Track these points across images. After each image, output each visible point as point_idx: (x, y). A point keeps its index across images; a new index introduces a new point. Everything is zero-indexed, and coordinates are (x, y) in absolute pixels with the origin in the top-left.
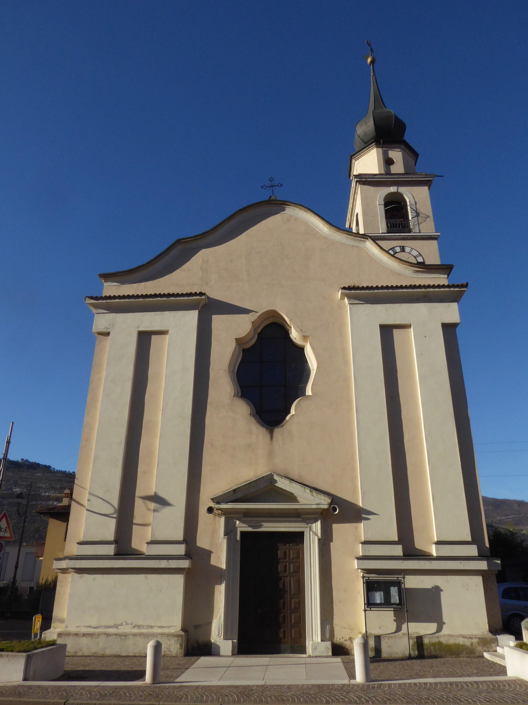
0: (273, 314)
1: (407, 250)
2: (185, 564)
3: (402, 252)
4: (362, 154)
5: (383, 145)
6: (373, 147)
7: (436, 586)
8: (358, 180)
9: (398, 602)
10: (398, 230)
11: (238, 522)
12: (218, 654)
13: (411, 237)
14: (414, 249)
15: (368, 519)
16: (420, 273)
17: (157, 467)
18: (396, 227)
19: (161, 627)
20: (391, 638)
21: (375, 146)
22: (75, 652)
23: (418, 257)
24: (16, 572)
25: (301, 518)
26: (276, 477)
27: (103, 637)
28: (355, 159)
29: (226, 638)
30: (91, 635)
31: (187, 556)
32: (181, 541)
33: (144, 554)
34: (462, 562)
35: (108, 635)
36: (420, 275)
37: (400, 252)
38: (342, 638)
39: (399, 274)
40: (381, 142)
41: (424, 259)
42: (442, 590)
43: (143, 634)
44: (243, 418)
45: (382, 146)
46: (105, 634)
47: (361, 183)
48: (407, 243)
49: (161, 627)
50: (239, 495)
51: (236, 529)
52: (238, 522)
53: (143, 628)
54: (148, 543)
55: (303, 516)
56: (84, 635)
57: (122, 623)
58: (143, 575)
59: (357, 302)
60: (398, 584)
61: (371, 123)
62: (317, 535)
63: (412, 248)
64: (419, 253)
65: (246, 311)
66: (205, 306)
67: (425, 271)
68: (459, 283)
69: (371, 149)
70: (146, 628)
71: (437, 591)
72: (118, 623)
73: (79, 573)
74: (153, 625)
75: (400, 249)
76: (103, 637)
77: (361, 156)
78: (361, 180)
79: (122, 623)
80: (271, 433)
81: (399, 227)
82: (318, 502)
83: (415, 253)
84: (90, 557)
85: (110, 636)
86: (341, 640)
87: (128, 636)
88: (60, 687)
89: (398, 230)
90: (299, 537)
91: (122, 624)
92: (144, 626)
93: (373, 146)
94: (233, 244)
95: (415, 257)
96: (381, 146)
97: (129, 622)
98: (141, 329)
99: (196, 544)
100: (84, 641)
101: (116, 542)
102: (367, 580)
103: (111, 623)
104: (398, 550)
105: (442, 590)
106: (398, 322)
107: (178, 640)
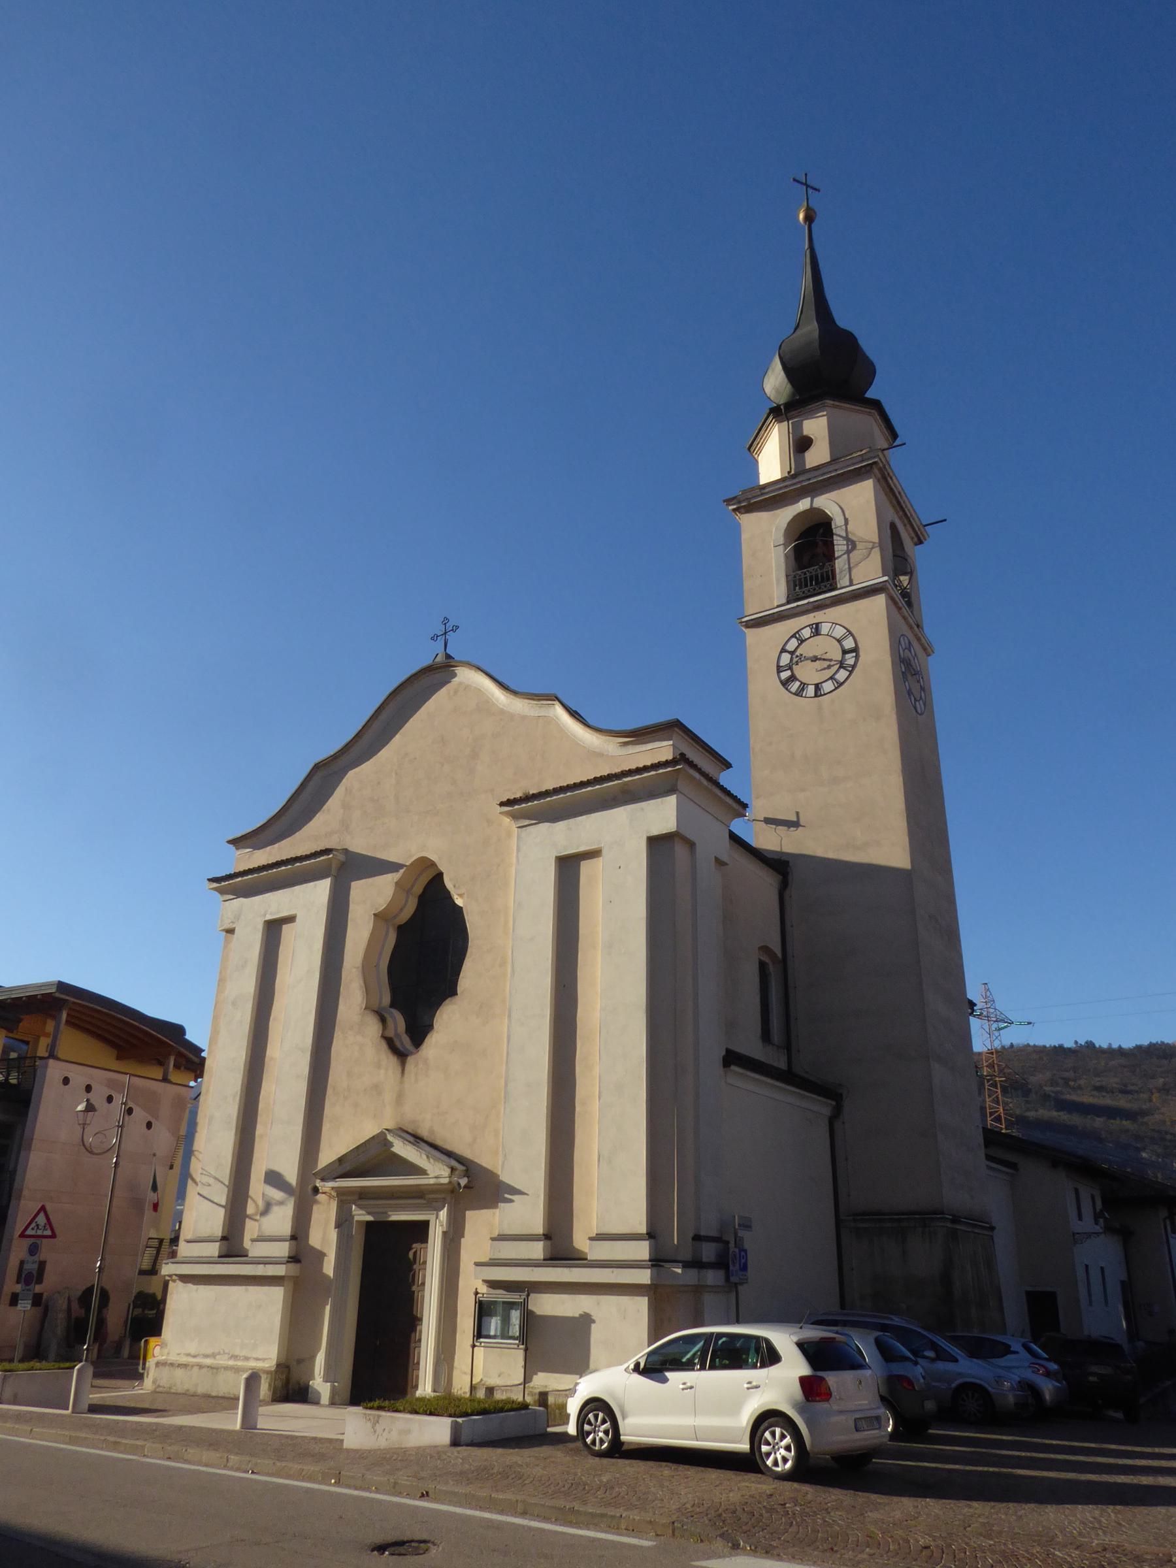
0: (425, 864)
1: (825, 628)
2: (644, 1277)
3: (814, 636)
4: (762, 441)
5: (788, 415)
6: (772, 423)
7: (584, 1312)
8: (735, 507)
9: (518, 1334)
10: (809, 591)
11: (354, 1206)
12: (316, 1402)
13: (862, 589)
14: (839, 625)
15: (511, 1201)
16: (631, 746)
17: (599, 1097)
18: (806, 586)
19: (257, 1359)
20: (506, 1392)
21: (774, 420)
22: (170, 1388)
23: (844, 638)
24: (270, 1284)
25: (425, 1199)
26: (390, 1138)
27: (196, 1369)
28: (755, 452)
29: (326, 1381)
30: (184, 1366)
31: (294, 1259)
32: (540, 1235)
33: (586, 1259)
34: (615, 1270)
35: (201, 1366)
36: (632, 749)
37: (811, 637)
38: (461, 1388)
39: (600, 755)
40: (781, 409)
41: (858, 639)
42: (594, 1322)
43: (234, 1368)
44: (373, 1044)
45: (786, 416)
46: (198, 1365)
47: (743, 510)
48: (815, 617)
49: (257, 1359)
50: (347, 1167)
51: (352, 1217)
52: (354, 1206)
53: (239, 1360)
54: (591, 1238)
55: (428, 1196)
56: (180, 1366)
57: (219, 1352)
58: (244, 1287)
59: (527, 822)
60: (524, 1306)
61: (777, 368)
62: (442, 1225)
63: (833, 623)
64: (848, 631)
65: (392, 867)
66: (343, 866)
67: (632, 741)
68: (634, 767)
69: (771, 428)
70: (242, 1360)
71: (586, 1321)
72: (217, 1351)
73: (184, 1282)
74: (249, 1356)
75: (810, 631)
76: (196, 1369)
77: (762, 443)
78: (739, 505)
79: (219, 1352)
80: (403, 1064)
81: (811, 585)
82: (436, 1174)
83: (839, 632)
84: (644, 1263)
85: (203, 1367)
86: (459, 1393)
87: (219, 1370)
88: (44, 1414)
89: (825, 586)
90: (420, 1231)
91: (219, 1354)
92: (240, 1357)
93: (771, 421)
94: (384, 753)
95: (839, 641)
96: (784, 416)
97: (226, 1351)
98: (269, 917)
99: (308, 1241)
100: (179, 1373)
101: (651, 1235)
102: (481, 1297)
103: (209, 1352)
104: (537, 1250)
105: (594, 1322)
106: (582, 848)
107: (267, 1378)
